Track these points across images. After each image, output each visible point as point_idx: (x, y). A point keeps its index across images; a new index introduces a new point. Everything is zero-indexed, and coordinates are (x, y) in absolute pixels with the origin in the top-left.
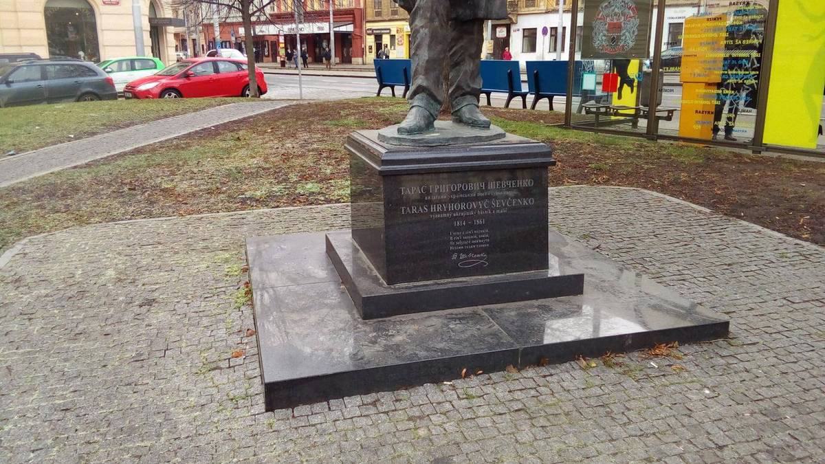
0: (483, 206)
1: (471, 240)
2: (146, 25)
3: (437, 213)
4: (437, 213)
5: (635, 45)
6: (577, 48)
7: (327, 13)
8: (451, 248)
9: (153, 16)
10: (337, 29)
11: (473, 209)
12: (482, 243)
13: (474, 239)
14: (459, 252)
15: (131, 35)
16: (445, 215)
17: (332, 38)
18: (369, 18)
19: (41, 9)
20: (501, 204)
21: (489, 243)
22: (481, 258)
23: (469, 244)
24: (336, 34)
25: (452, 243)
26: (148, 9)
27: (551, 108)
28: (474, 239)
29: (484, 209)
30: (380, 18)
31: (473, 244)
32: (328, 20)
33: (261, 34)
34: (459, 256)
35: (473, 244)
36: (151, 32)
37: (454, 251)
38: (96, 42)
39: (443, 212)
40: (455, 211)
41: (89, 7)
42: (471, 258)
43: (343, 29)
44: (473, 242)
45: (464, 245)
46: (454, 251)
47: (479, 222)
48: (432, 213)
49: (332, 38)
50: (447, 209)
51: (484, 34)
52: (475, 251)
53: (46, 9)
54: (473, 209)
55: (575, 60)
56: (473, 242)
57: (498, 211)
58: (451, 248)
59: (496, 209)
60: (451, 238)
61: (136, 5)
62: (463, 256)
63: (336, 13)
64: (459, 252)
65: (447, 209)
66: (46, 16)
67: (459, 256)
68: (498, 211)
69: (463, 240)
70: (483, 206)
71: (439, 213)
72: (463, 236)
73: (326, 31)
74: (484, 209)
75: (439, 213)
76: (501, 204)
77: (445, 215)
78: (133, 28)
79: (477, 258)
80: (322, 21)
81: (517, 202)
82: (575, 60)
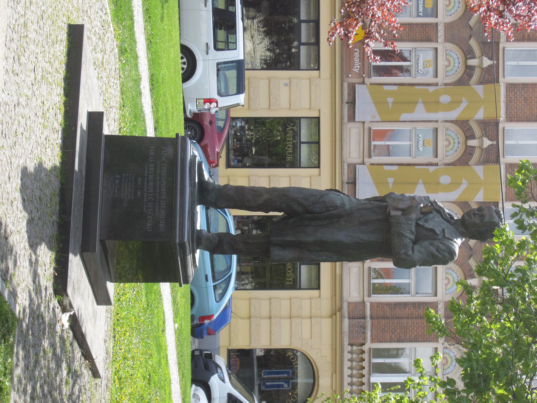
0: (149, 197)
3: (148, 167)
4: (148, 167)
5: (486, 137)
6: (312, 61)
8: (124, 175)
19: (295, 345)
20: (150, 208)
34: (117, 179)
38: (490, 147)
40: (148, 178)
44: (126, 189)
47: (139, 193)
48: (148, 165)
50: (150, 174)
55: (106, 131)
56: (126, 189)
57: (145, 206)
59: (147, 205)
65: (150, 174)
67: (117, 179)
68: (145, 206)
70: (149, 197)
76: (150, 208)
79: (114, 190)
82: (106, 131)
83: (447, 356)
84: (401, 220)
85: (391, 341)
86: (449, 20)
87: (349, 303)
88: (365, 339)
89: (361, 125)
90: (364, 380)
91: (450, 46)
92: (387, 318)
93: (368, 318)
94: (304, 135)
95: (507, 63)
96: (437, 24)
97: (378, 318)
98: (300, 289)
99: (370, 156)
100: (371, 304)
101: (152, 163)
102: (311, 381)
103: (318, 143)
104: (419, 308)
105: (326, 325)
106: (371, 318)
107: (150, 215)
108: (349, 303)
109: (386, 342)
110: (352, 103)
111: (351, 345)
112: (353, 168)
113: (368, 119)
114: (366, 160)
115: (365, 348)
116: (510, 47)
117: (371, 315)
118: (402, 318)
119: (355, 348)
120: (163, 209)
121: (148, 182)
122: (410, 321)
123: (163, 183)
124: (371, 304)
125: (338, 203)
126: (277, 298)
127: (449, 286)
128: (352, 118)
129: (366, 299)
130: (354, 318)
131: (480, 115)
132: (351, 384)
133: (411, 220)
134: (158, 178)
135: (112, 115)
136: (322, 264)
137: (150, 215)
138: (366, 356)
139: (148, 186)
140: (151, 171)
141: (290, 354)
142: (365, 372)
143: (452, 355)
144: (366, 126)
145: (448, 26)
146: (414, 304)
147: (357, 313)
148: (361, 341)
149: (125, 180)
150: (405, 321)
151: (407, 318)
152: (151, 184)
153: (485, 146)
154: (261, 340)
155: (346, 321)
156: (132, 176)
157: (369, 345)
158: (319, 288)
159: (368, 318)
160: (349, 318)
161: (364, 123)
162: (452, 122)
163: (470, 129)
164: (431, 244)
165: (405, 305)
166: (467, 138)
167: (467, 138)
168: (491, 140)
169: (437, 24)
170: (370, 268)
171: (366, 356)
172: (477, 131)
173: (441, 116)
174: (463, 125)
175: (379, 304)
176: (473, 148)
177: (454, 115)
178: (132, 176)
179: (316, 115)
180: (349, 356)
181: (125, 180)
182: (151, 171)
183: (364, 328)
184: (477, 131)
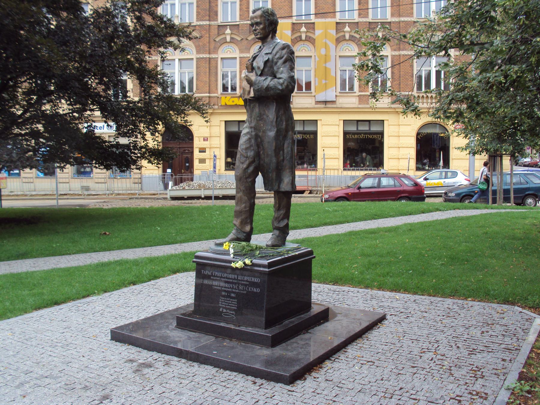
19: (414, 134)
22: (233, 314)
25: (220, 303)
47: (233, 295)
52: (230, 310)
53: (418, 134)
59: (241, 290)
62: (225, 311)
64: (223, 308)
86: (238, 51)
87: (359, 104)
89: (338, 98)
91: (220, 51)
92: (400, 83)
94: (353, 128)
95: (229, 20)
96: (240, 57)
99: (311, 93)
102: (438, 125)
103: (304, 121)
107: (248, 289)
110: (326, 102)
112: (318, 102)
113: (334, 94)
114: (313, 95)
115: (416, 95)
116: (220, 20)
117: (212, 97)
128: (333, 102)
129: (356, 94)
131: (333, 32)
135: (333, 230)
136: (295, 119)
138: (421, 95)
141: (419, 137)
144: (338, 94)
145: (241, 51)
153: (305, 30)
154: (411, 152)
157: (415, 93)
161: (336, 96)
162: (336, 47)
163: (296, 38)
164: (276, 63)
166: (301, 40)
167: (301, 40)
168: (345, 26)
169: (240, 57)
170: (340, 93)
171: (421, 95)
172: (341, 34)
173: (332, 53)
174: (339, 41)
176: (306, 36)
177: (332, 46)
179: (224, 123)
184: (298, 34)
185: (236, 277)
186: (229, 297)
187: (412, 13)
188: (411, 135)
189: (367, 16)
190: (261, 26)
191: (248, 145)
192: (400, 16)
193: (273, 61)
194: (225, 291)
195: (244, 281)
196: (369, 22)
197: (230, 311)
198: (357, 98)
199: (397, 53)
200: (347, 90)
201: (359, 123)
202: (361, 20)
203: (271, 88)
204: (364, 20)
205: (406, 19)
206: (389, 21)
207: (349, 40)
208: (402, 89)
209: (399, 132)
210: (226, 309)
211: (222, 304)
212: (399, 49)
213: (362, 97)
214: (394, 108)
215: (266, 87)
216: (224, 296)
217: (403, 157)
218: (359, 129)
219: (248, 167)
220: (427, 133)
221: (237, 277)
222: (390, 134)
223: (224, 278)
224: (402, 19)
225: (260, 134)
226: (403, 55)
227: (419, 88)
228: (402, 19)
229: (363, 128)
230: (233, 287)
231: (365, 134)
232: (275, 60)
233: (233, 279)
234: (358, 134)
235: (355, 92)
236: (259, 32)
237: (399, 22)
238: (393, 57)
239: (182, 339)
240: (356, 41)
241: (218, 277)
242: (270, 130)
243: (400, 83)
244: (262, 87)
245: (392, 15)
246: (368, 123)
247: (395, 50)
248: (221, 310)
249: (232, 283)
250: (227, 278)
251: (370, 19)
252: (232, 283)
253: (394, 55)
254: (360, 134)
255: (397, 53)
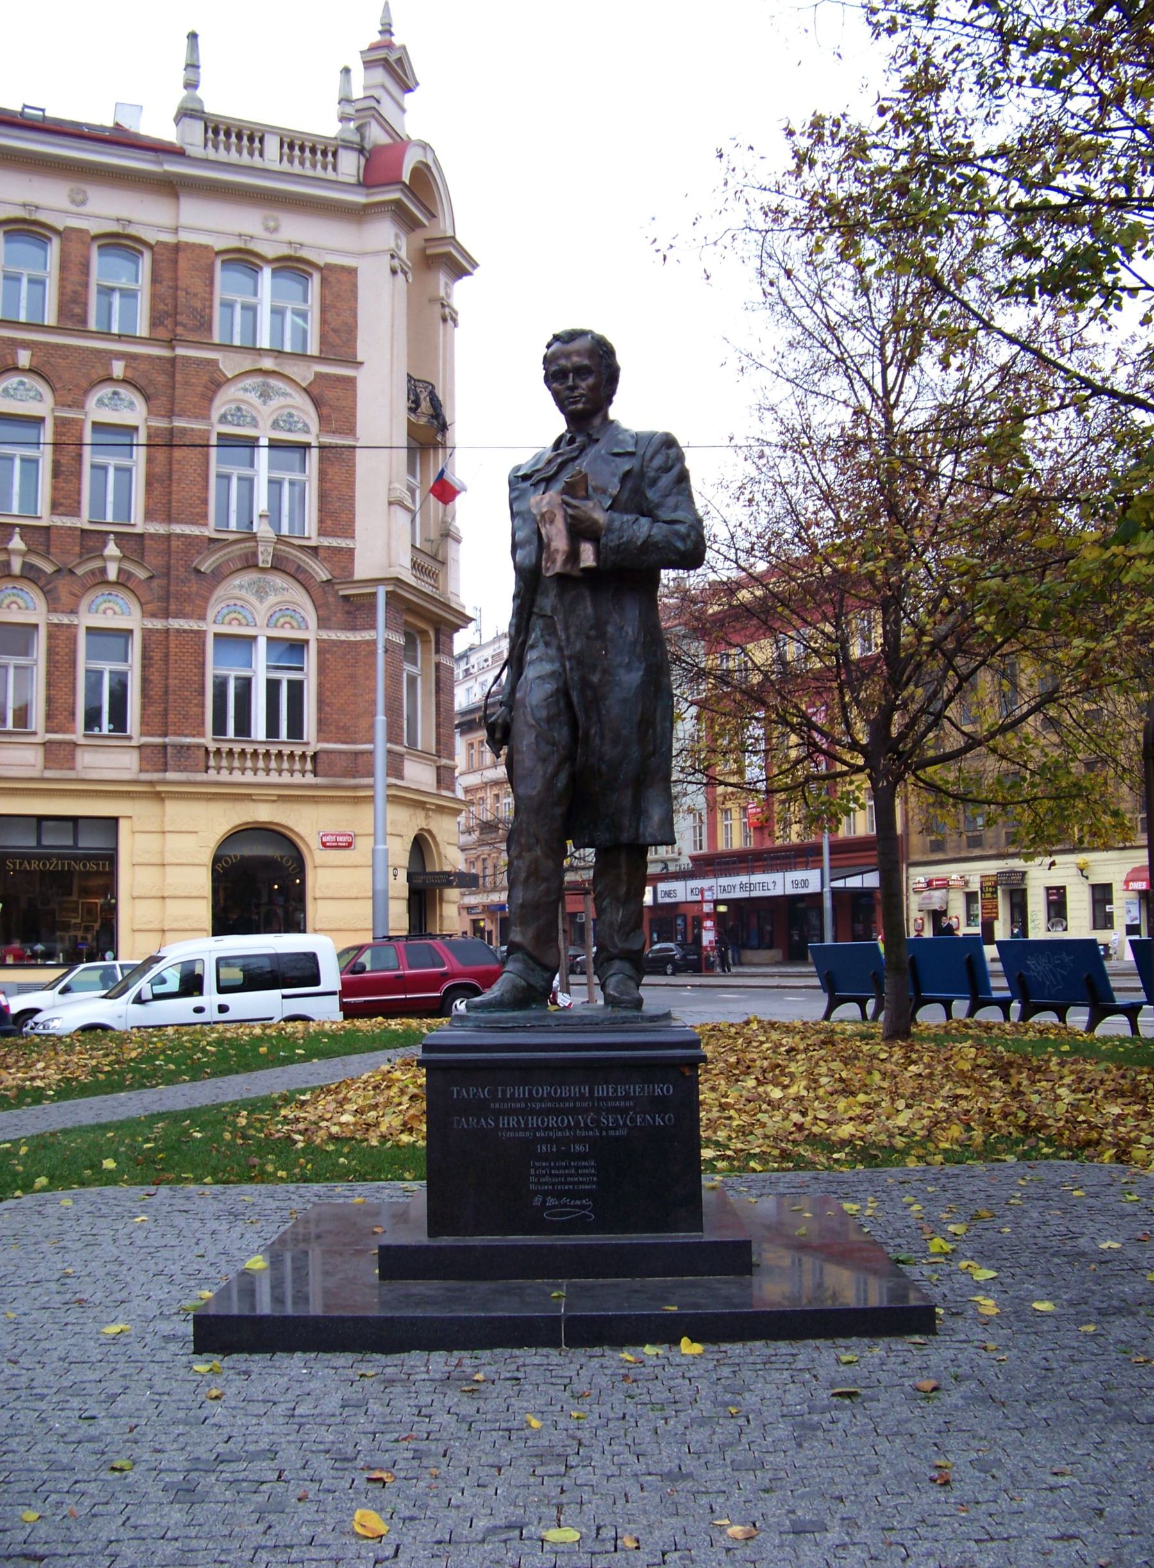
1: (566, 1176)
2: (400, 886)
3: (509, 1129)
4: (509, 1129)
7: (817, 850)
8: (532, 1187)
9: (418, 869)
10: (839, 884)
11: (569, 1127)
12: (582, 1183)
13: (571, 1175)
14: (545, 1194)
15: (368, 906)
16: (521, 1134)
17: (827, 903)
18: (915, 857)
19: (207, 857)
20: (616, 1120)
21: (597, 1183)
22: (583, 1207)
23: (561, 1183)
24: (835, 892)
25: (532, 1179)
26: (407, 855)
27: (1135, 1029)
28: (571, 1175)
29: (587, 1128)
30: (977, 852)
31: (570, 1183)
32: (818, 864)
33: (668, 900)
34: (544, 1201)
35: (570, 1183)
36: (409, 900)
37: (536, 1192)
39: (519, 1129)
40: (538, 1129)
41: (295, 854)
42: (565, 1206)
43: (854, 882)
45: (553, 1184)
46: (536, 1192)
47: (579, 1148)
49: (827, 903)
50: (526, 1124)
51: (778, 891)
52: (573, 1194)
53: (216, 860)
54: (569, 1127)
57: (612, 1133)
58: (532, 1187)
59: (608, 1128)
60: (532, 1171)
61: (380, 847)
62: (551, 1201)
63: (838, 848)
64: (545, 1194)
65: (526, 1124)
66: (214, 871)
68: (612, 1133)
69: (551, 1175)
71: (514, 1130)
72: (551, 1168)
73: (814, 887)
74: (587, 1128)
75: (514, 1130)
77: (521, 1134)
78: (370, 894)
79: (575, 1206)
80: (806, 866)
81: (644, 1120)
83: (227, 619)
84: (611, 544)
85: (203, 706)
87: (141, 771)
88: (198, 746)
90: (262, 750)
92: (166, 710)
93: (167, 740)
97: (166, 724)
98: (116, 849)
100: (142, 734)
101: (496, 1121)
104: (151, 658)
105: (173, 808)
106: (166, 735)
107: (633, 1120)
108: (141, 771)
109: (203, 714)
111: (207, 768)
115: (212, 747)
118: (167, 686)
119: (212, 763)
120: (616, 1090)
121: (547, 1129)
122: (172, 674)
123: (549, 1093)
124: (142, 734)
125: (549, 687)
126: (132, 887)
127: (117, 609)
129: (134, 743)
130: (166, 764)
132: (268, 771)
133: (611, 522)
134: (538, 1106)
137: (633, 1120)
138: (225, 747)
139: (560, 1129)
140: (518, 1122)
142: (249, 749)
143: (225, 611)
146: (144, 667)
147: (158, 757)
148: (202, 752)
149: (546, 1183)
150: (171, 682)
151: (167, 678)
152: (552, 1121)
155: (171, 776)
156: (536, 1168)
157: (208, 740)
158: (115, 820)
159: (167, 740)
160: (165, 771)
164: (654, 482)
165: (145, 680)
171: (225, 747)
175: (144, 721)
178: (536, 1168)
180: (224, 772)
181: (546, 1183)
182: (518, 1122)
183: (182, 746)
185: (586, 1090)
186: (569, 1156)
187: (205, 516)
188: (197, 861)
189: (75, 512)
190: (591, 381)
191: (554, 710)
192: (169, 519)
193: (642, 474)
194: (548, 1140)
195: (616, 1099)
196: (83, 531)
197: (574, 1198)
198: (41, 751)
199: (158, 624)
200: (10, 726)
201: (45, 823)
202: (59, 521)
203: (655, 544)
204: (68, 522)
205: (188, 530)
206: (138, 530)
207: (22, 577)
208: (171, 728)
209: (162, 853)
210: (559, 1195)
211: (538, 1183)
212: (167, 615)
213: (54, 747)
214: (151, 783)
215: (645, 542)
216: (545, 1157)
217: (175, 926)
218: (45, 842)
219: (555, 775)
220: (242, 857)
221: (591, 1091)
222: (137, 860)
223: (542, 1100)
224: (177, 529)
225: (595, 678)
226: (178, 630)
227: (220, 728)
228: (177, 529)
229: (55, 839)
230: (577, 1123)
231: (60, 857)
232: (652, 474)
233: (575, 1100)
234: (39, 857)
235: (34, 733)
236: (582, 395)
237: (169, 537)
238: (147, 634)
239: (426, 1297)
240: (42, 583)
241: (519, 1100)
242: (629, 668)
243: (166, 710)
244: (630, 541)
245: (149, 516)
246: (71, 824)
247: (154, 615)
248: (537, 1201)
249: (574, 1111)
250: (550, 1098)
251: (83, 521)
252: (574, 1111)
253: (150, 630)
254: (48, 857)
255: (158, 624)
